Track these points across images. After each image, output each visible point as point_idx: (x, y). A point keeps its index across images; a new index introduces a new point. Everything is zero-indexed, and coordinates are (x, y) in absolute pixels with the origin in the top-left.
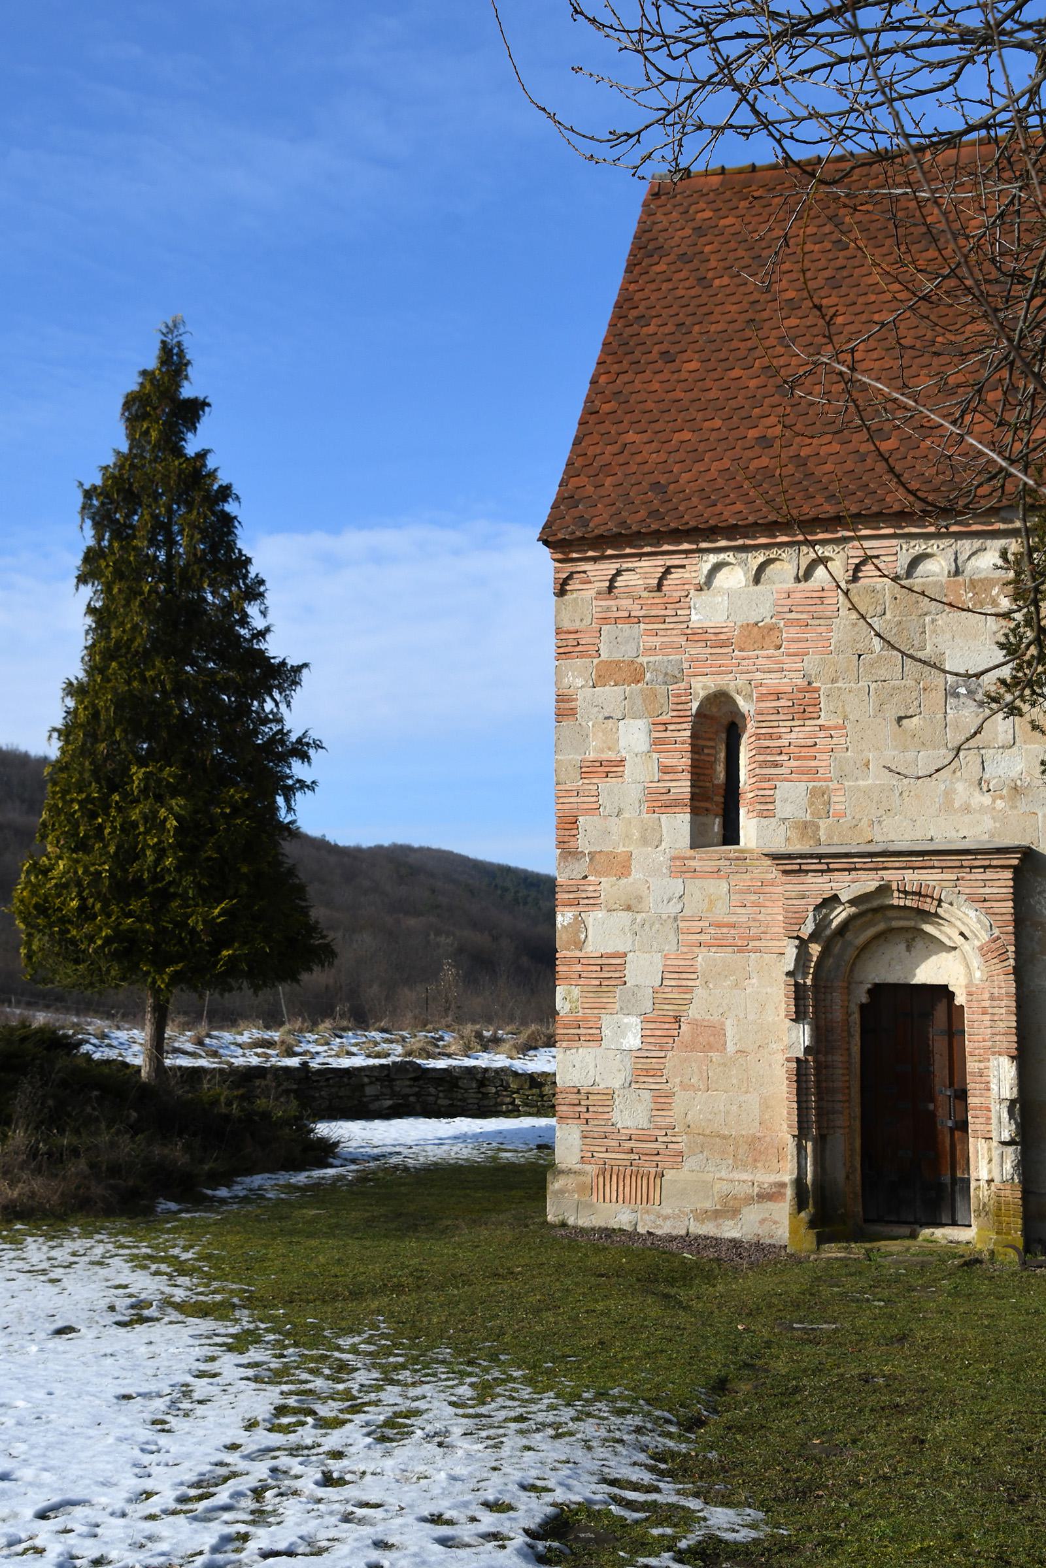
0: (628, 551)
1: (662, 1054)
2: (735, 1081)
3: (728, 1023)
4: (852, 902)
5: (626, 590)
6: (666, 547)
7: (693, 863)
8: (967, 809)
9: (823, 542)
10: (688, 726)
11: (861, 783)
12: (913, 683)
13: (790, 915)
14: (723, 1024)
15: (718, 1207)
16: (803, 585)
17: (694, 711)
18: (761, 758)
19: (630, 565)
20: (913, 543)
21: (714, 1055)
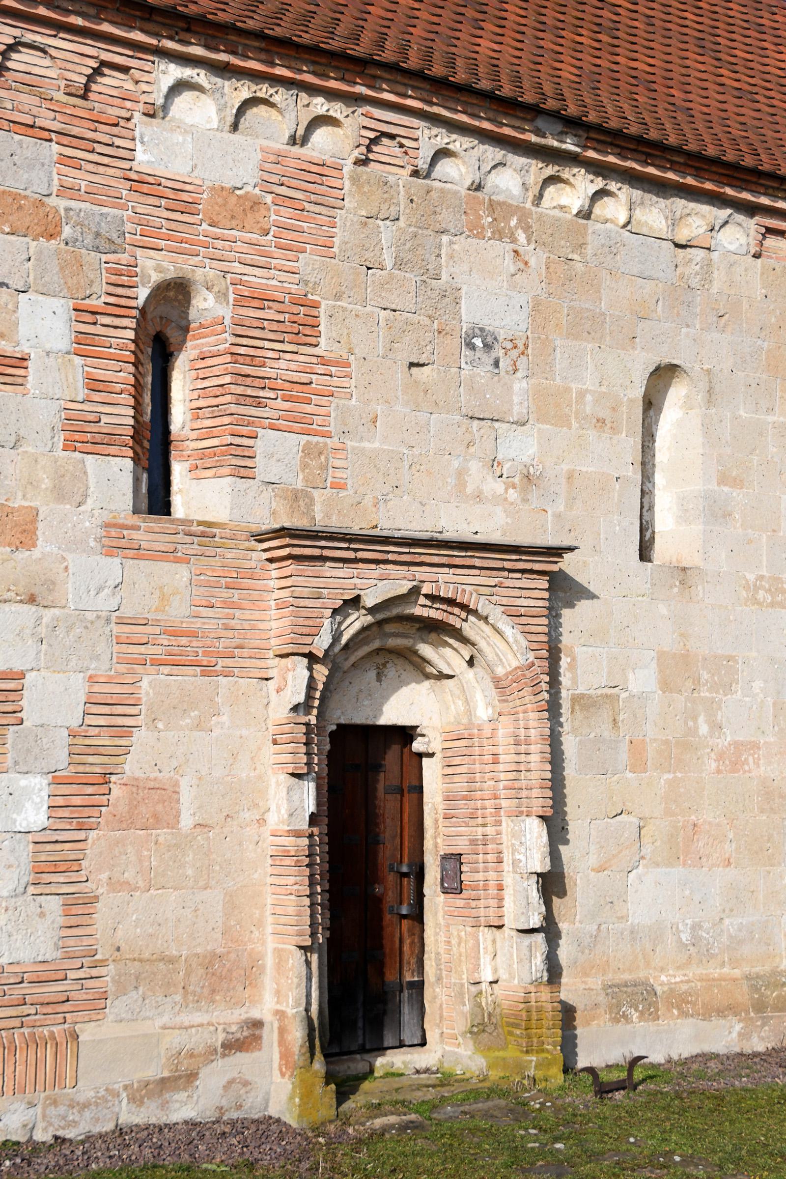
0: (42, 11)
1: (81, 835)
2: (190, 872)
3: (184, 783)
4: (371, 611)
5: (27, 79)
6: (106, 27)
7: (135, 535)
8: (479, 497)
9: (332, 95)
10: (132, 323)
11: (365, 444)
12: (427, 321)
13: (301, 621)
14: (177, 784)
15: (166, 1074)
16: (296, 150)
17: (141, 302)
18: (239, 390)
19: (38, 38)
20: (435, 131)
21: (163, 834)
